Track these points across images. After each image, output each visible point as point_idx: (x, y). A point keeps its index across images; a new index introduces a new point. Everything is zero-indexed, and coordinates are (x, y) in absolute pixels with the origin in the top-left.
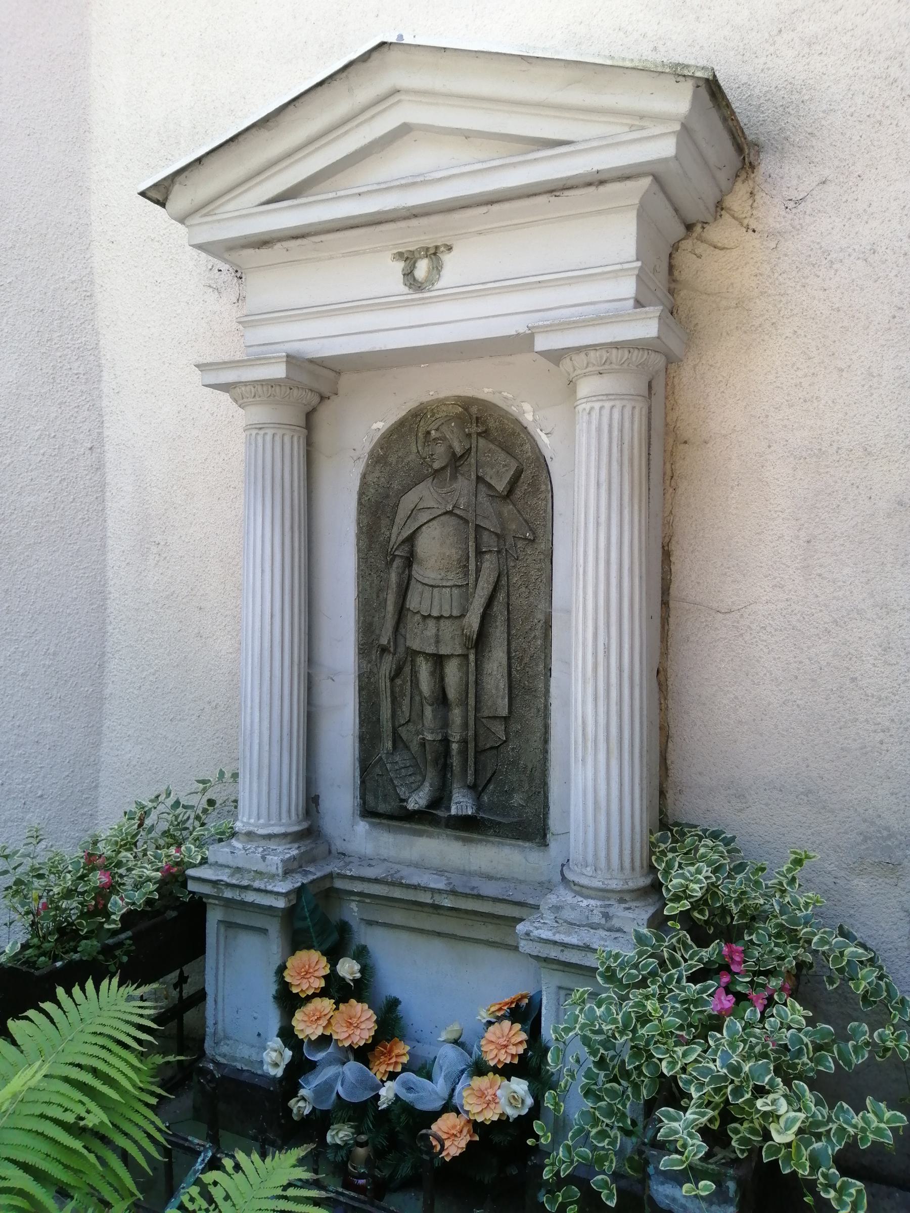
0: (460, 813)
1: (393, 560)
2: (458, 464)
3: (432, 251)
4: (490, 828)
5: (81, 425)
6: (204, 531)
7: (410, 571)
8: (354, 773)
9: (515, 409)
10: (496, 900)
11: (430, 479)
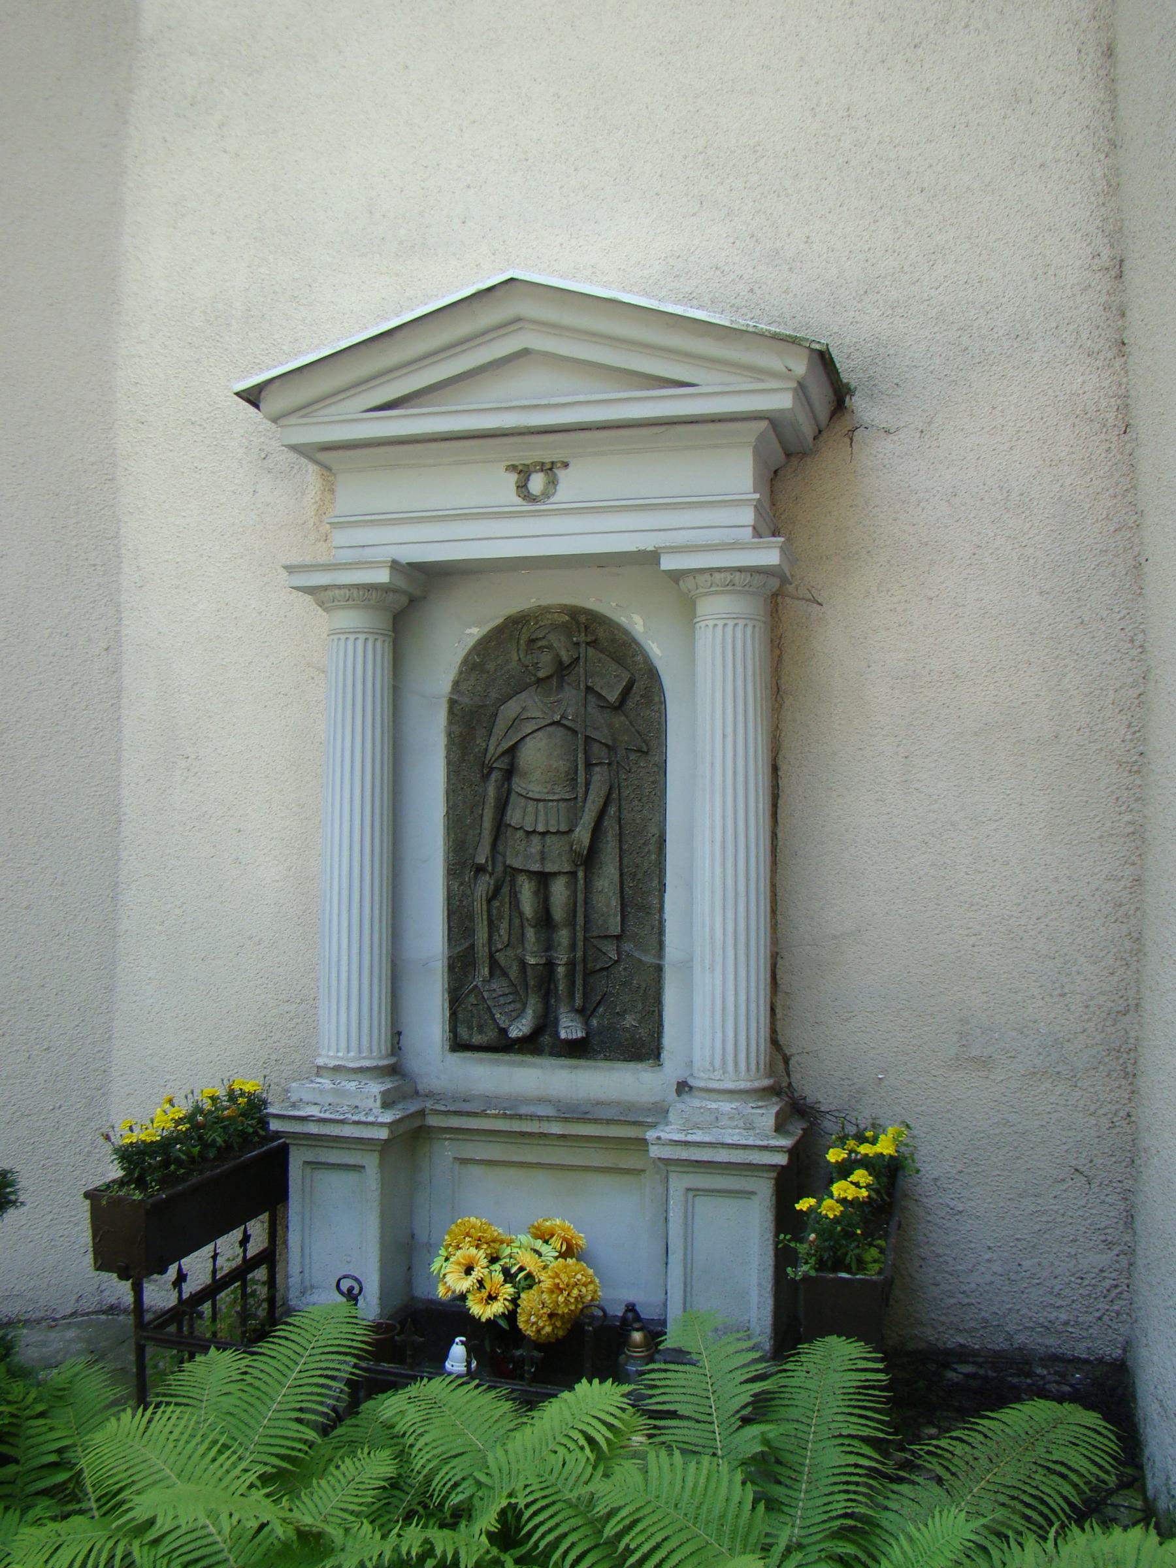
0: (570, 1037)
1: (489, 773)
2: (565, 673)
3: (548, 466)
4: (599, 1052)
5: (96, 622)
7: (510, 784)
8: (443, 1005)
9: (624, 620)
11: (533, 688)
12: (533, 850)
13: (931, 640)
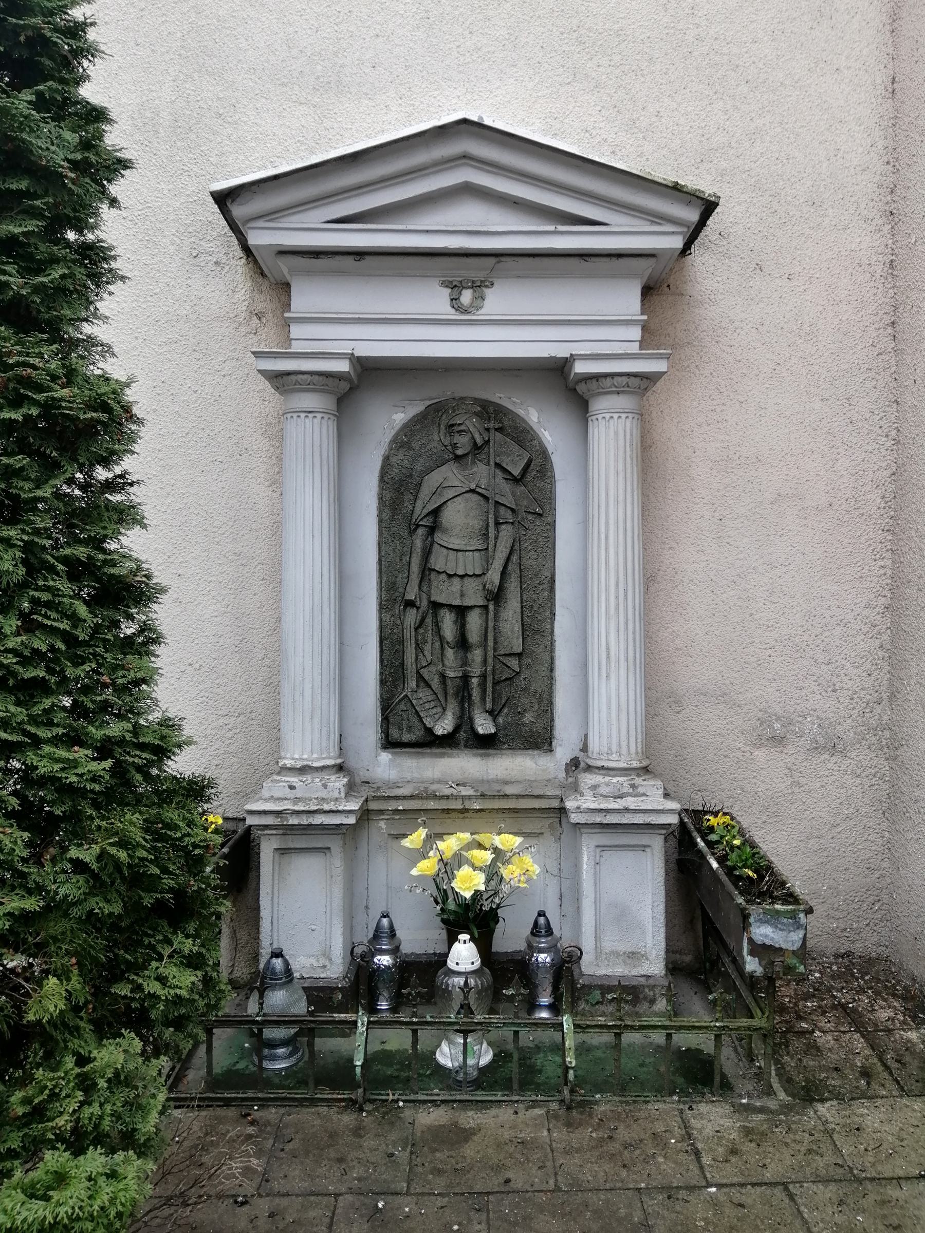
1: (416, 529)
4: (504, 743)
6: (185, 501)
7: (432, 538)
10: (518, 797)
12: (454, 589)
13: (741, 433)
